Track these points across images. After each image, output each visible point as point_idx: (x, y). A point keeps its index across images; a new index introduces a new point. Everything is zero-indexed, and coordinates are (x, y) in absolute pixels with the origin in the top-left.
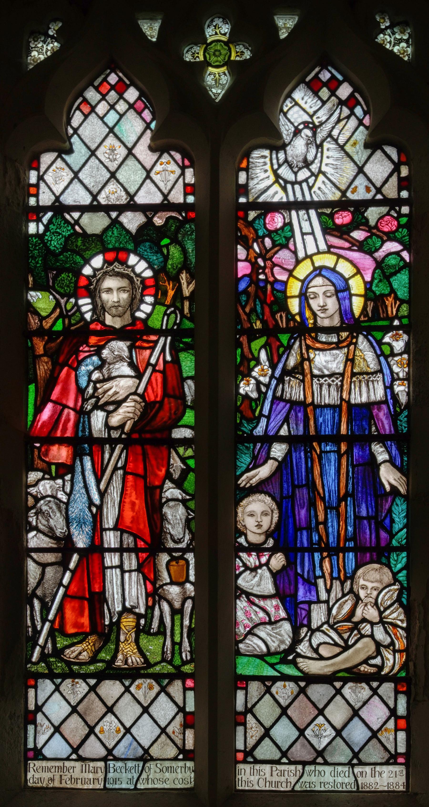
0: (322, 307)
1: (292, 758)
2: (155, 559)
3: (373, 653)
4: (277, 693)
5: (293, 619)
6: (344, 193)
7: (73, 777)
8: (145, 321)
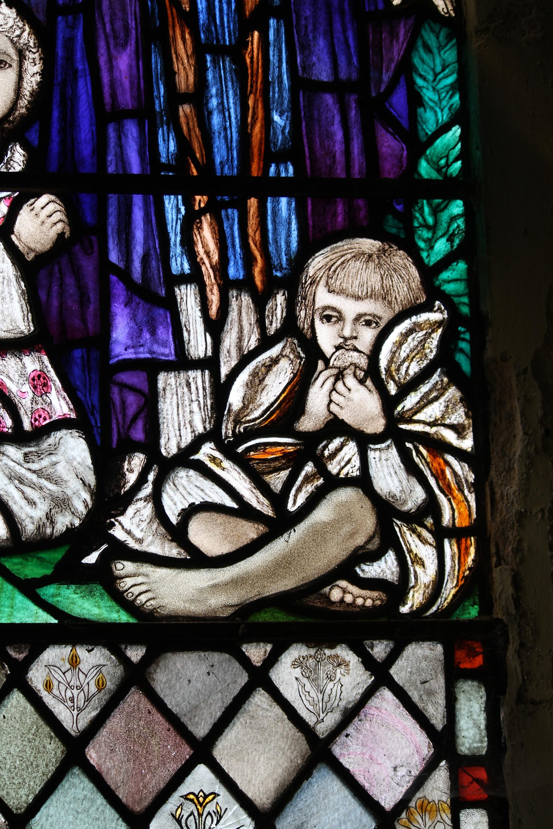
3: (370, 539)
4: (48, 686)
5: (96, 420)
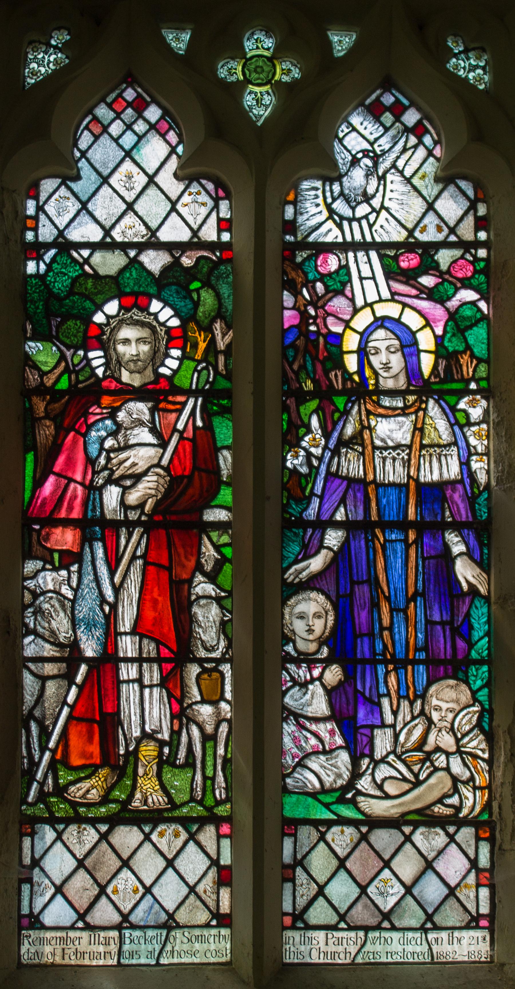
0: (385, 364)
1: (352, 922)
2: (182, 671)
3: (450, 790)
4: (333, 840)
6: (411, 233)
7: (78, 950)
8: (170, 379)
